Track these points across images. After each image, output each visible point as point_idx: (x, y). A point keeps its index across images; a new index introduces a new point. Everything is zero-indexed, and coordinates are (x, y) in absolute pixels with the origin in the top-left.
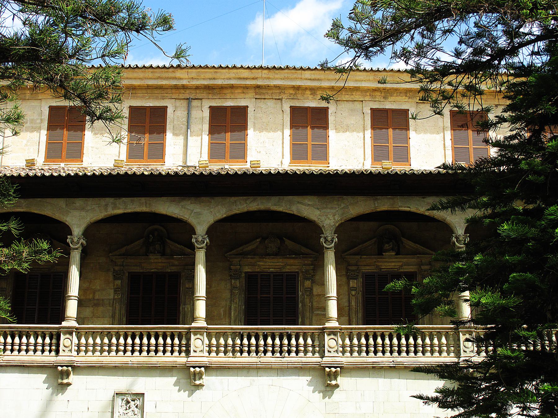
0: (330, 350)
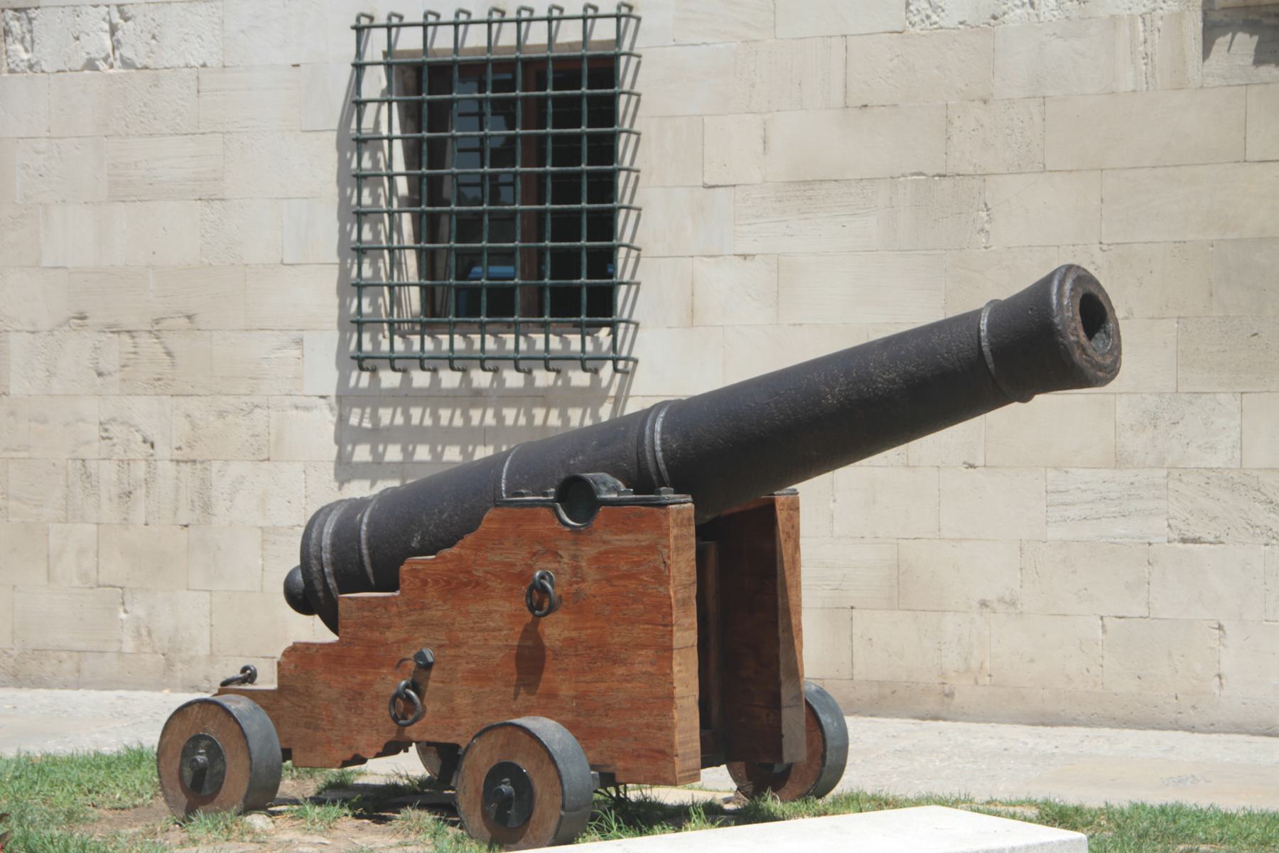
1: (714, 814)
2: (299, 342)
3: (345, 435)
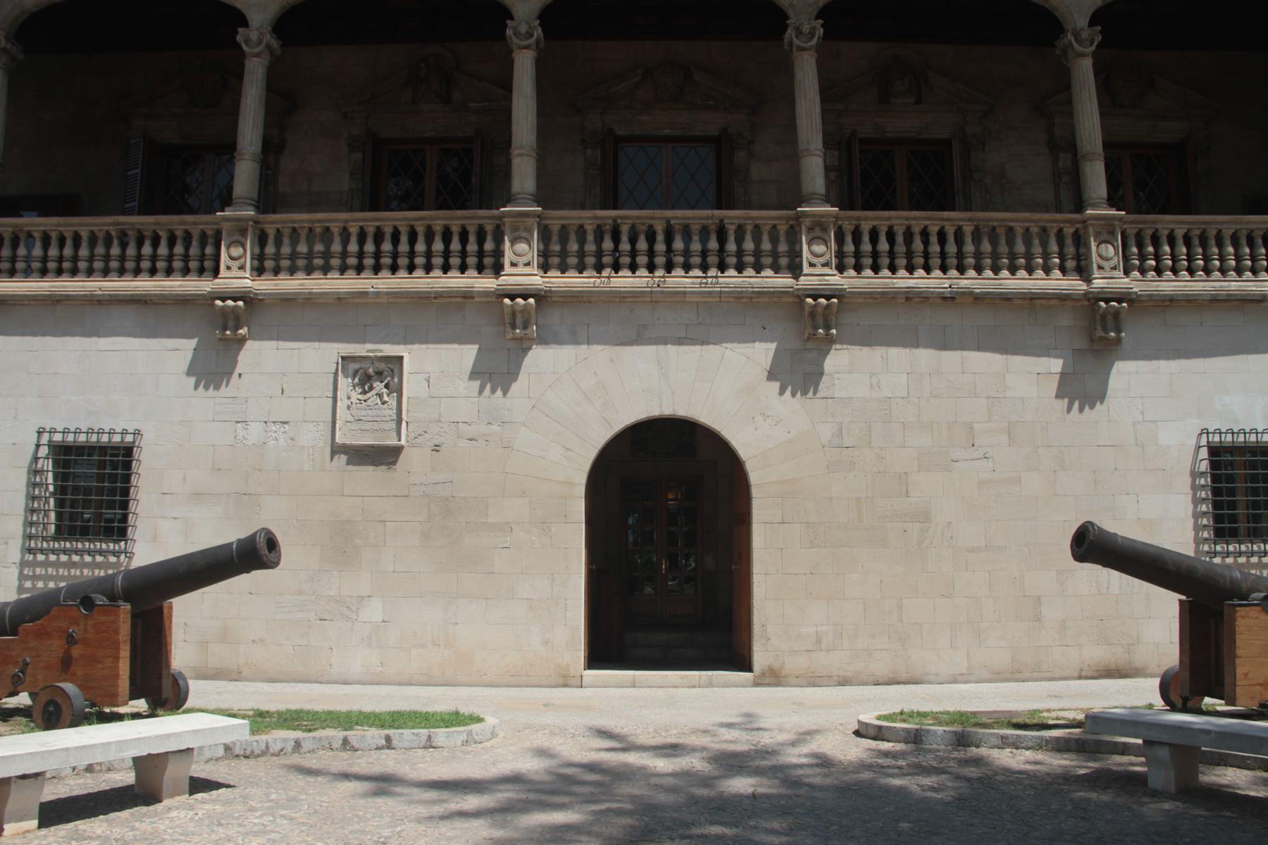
0: (815, 260)
1: (136, 716)
2: (6, 543)
3: (22, 577)
